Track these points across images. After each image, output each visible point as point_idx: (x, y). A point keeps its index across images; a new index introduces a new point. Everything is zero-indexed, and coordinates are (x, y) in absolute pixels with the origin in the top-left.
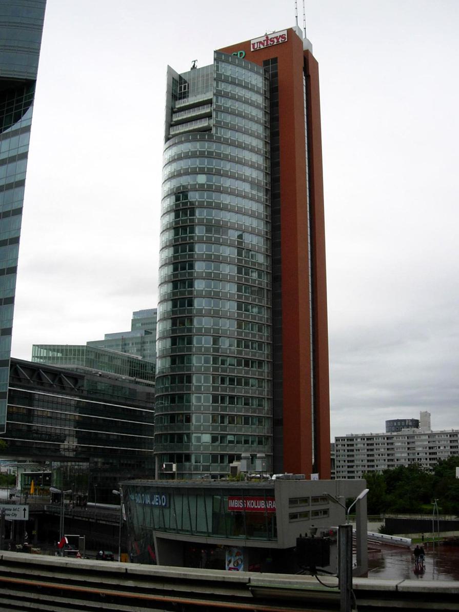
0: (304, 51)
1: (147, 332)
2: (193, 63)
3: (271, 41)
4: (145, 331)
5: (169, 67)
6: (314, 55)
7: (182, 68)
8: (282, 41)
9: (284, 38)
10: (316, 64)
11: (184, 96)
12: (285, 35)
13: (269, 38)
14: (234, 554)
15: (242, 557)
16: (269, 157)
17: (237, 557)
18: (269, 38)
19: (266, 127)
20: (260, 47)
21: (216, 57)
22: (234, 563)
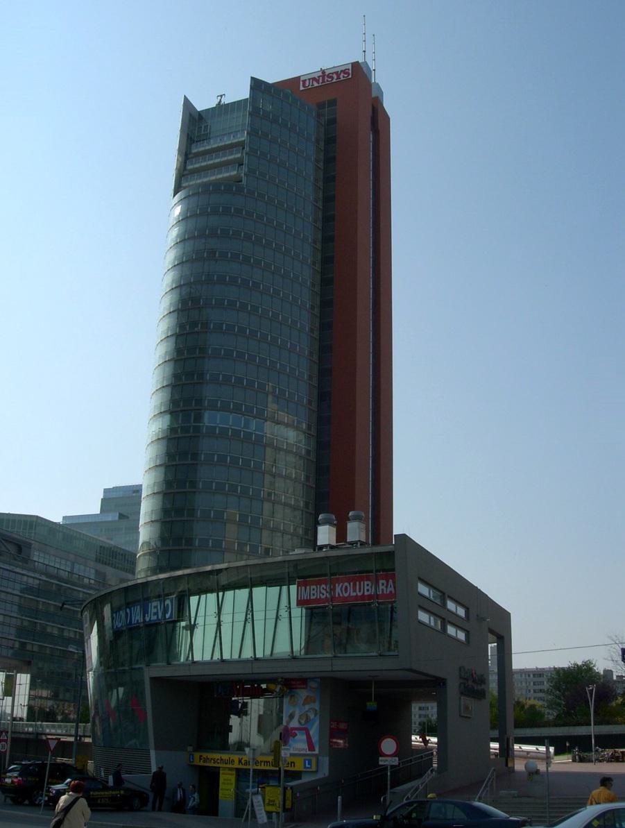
0: (373, 98)
1: (122, 516)
2: (219, 98)
4: (120, 514)
6: (384, 105)
7: (203, 103)
8: (344, 77)
10: (387, 119)
11: (205, 138)
12: (349, 69)
13: (327, 74)
14: (301, 701)
15: (317, 706)
17: (307, 707)
18: (327, 74)
20: (313, 85)
22: (300, 717)
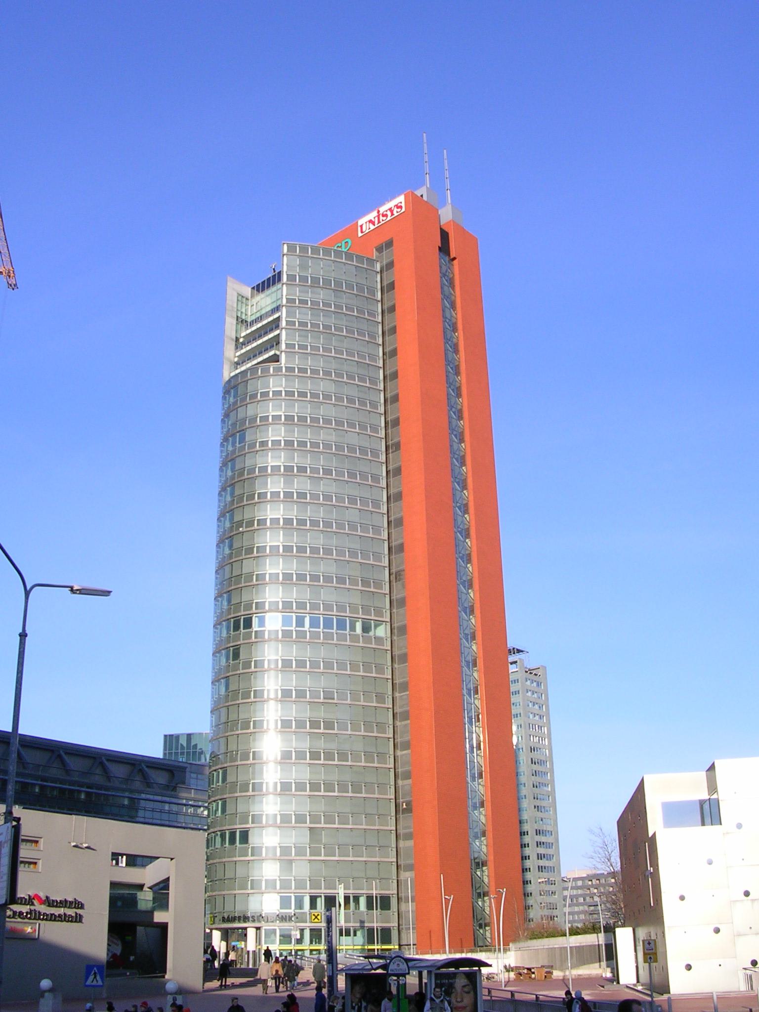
3: (383, 216)
9: (401, 207)
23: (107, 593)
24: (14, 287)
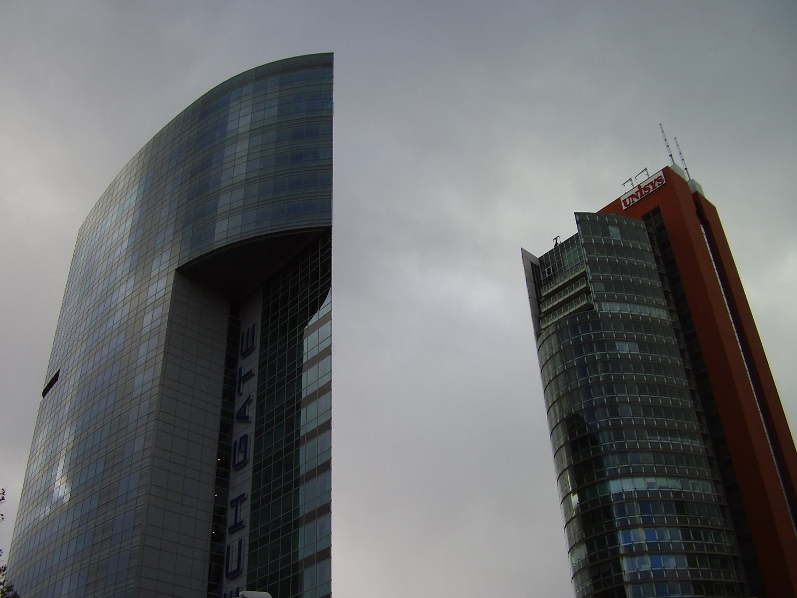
0: (693, 194)
2: (555, 240)
5: (524, 252)
6: (706, 197)
7: (541, 249)
8: (659, 185)
9: (661, 180)
10: (713, 209)
12: (661, 176)
16: (675, 309)
18: (643, 187)
19: (716, 483)
20: (633, 202)
21: (578, 219)
23: (45, 393)
24: (2, 515)
